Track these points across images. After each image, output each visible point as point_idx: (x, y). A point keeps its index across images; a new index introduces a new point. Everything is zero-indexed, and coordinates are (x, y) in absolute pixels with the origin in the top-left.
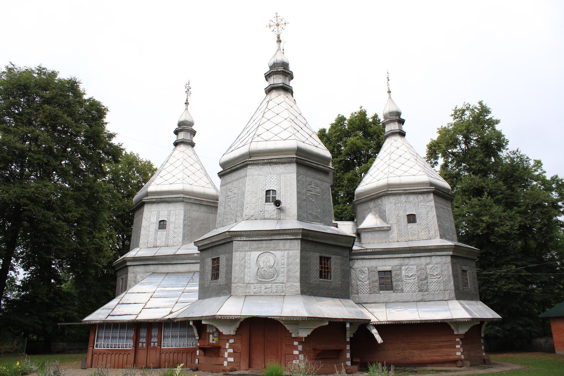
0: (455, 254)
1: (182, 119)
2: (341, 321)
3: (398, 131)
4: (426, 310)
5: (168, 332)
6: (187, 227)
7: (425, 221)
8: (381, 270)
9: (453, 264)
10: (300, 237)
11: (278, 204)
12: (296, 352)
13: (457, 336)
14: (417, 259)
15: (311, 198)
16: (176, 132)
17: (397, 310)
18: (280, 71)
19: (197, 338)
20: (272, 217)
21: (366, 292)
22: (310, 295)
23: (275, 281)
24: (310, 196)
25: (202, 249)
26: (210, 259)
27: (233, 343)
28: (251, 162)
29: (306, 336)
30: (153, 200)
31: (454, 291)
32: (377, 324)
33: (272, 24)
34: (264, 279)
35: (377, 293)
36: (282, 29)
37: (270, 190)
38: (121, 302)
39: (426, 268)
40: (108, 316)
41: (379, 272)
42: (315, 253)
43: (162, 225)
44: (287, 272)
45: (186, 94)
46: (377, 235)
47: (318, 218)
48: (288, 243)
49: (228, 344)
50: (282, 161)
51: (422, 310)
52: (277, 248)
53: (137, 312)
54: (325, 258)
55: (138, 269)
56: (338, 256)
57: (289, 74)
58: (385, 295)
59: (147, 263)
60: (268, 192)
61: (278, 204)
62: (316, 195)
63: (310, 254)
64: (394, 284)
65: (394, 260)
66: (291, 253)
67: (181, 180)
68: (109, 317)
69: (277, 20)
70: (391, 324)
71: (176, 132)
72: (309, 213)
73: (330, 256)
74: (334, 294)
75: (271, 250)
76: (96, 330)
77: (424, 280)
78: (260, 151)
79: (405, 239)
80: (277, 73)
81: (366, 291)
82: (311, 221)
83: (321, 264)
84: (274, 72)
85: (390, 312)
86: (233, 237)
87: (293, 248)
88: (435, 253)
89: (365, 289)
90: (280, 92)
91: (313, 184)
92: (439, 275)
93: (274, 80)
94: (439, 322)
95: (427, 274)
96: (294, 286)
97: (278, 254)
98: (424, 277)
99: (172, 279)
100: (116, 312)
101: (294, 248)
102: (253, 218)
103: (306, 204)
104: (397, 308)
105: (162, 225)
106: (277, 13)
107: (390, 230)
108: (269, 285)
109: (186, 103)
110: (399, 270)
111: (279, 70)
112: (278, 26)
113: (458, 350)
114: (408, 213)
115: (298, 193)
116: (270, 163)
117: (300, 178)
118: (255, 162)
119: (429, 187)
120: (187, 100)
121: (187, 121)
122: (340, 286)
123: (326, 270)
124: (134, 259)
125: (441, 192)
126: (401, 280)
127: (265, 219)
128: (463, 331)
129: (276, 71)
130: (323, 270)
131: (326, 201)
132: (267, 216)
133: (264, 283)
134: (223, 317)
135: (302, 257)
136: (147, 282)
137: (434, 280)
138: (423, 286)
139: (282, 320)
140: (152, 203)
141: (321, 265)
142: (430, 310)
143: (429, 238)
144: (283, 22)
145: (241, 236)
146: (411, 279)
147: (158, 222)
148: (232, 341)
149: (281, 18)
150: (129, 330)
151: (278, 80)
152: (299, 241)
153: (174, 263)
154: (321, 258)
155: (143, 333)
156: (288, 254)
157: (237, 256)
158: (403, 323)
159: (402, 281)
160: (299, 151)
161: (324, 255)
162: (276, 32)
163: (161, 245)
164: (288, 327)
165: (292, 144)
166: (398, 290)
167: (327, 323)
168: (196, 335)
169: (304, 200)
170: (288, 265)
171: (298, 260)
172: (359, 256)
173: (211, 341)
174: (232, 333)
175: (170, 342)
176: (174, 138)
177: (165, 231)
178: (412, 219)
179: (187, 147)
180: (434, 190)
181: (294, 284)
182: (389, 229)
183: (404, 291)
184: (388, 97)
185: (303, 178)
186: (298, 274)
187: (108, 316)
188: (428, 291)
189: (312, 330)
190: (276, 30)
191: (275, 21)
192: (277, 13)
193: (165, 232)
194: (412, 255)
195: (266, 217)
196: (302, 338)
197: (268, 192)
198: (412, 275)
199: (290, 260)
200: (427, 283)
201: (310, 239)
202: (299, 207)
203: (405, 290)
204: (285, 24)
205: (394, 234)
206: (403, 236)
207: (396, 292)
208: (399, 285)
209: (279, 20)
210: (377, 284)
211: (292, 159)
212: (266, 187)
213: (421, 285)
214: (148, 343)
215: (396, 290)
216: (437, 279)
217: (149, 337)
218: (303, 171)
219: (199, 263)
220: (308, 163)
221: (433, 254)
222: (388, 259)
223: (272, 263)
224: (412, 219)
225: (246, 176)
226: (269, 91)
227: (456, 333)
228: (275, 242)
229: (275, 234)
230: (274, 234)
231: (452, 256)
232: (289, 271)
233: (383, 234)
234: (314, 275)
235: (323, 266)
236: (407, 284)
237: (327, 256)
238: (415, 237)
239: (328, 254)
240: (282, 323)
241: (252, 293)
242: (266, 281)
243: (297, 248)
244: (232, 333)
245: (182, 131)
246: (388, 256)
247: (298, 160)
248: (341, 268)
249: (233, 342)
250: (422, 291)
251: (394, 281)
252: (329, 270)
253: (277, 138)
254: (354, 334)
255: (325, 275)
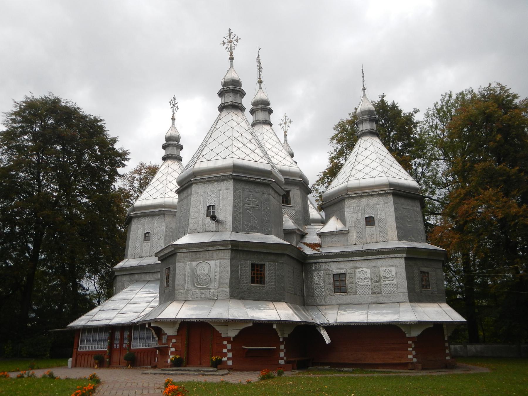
0: (409, 256)
1: (168, 135)
2: (266, 322)
3: (369, 130)
4: (376, 312)
5: (136, 334)
6: (169, 237)
7: (383, 223)
8: (335, 273)
9: (407, 266)
10: (230, 248)
11: (214, 219)
12: (225, 351)
13: (411, 339)
14: (337, 263)
15: (248, 211)
16: (164, 147)
17: (348, 312)
18: (229, 90)
19: (157, 339)
20: (212, 230)
21: (365, 293)
22: (240, 299)
23: (209, 288)
24: (247, 208)
25: (162, 259)
26: (165, 268)
27: (175, 342)
28: (194, 182)
29: (234, 336)
30: (139, 215)
31: (407, 294)
32: (326, 325)
33: (225, 41)
34: (201, 285)
35: (332, 296)
36: (234, 46)
37: (210, 206)
38: (102, 309)
39: (380, 271)
40: (89, 321)
41: (334, 275)
42: (246, 261)
43: (147, 236)
44: (219, 279)
45: (171, 110)
46: (336, 239)
47: (255, 228)
48: (220, 254)
49: (171, 344)
50: (221, 178)
51: (373, 312)
52: (211, 258)
53: (113, 316)
54: (257, 265)
55: (125, 278)
56: (272, 263)
57: (240, 91)
58: (340, 297)
59: (131, 272)
60: (209, 207)
61: (214, 219)
62: (253, 207)
63: (241, 262)
64: (348, 286)
65: (348, 263)
66: (223, 262)
67: (164, 194)
68: (89, 322)
69: (230, 37)
70: (337, 326)
71: (164, 147)
72: (245, 225)
73: (264, 263)
74: (267, 297)
75: (207, 260)
76: (132, 331)
77: (378, 282)
78: (202, 170)
79: (363, 242)
80: (227, 91)
81: (392, 288)
82: (247, 232)
83: (252, 270)
84: (224, 91)
85: (341, 314)
86: (177, 249)
87: (224, 258)
88: (388, 255)
89: (394, 289)
90: (229, 110)
91: (251, 197)
92: (392, 277)
93: (225, 99)
94: (386, 324)
95: (380, 276)
96: (224, 291)
97: (212, 263)
98: (377, 280)
99: (151, 286)
100: (96, 317)
101: (225, 258)
102: (196, 231)
103: (243, 217)
104: (349, 311)
105: (147, 236)
106: (230, 30)
107: (349, 233)
108: (203, 291)
109: (258, 82)
110: (353, 272)
111: (228, 89)
112: (231, 43)
113: (410, 353)
114: (366, 216)
115: (234, 207)
116: (210, 181)
117: (237, 193)
118: (198, 181)
119: (389, 189)
120: (260, 78)
121: (172, 136)
122: (274, 290)
123: (259, 276)
124: (122, 269)
125: (402, 193)
126: (354, 283)
127: (206, 232)
128: (415, 333)
129: (226, 90)
130: (256, 276)
131: (265, 211)
132: (208, 229)
133: (201, 289)
134: (161, 320)
135: (231, 266)
136: (129, 289)
137: (387, 283)
138: (376, 288)
139: (210, 322)
140: (139, 217)
141: (253, 272)
142: (380, 312)
143: (387, 240)
144: (235, 38)
145: (182, 248)
146: (364, 282)
147: (143, 235)
148: (174, 341)
149: (233, 34)
150: (135, 332)
151: (229, 99)
152: (230, 251)
153: (154, 271)
154: (253, 265)
155: (126, 334)
156: (220, 263)
157: (179, 265)
158: (351, 325)
159: (356, 283)
160: (236, 168)
161: (256, 262)
162: (229, 49)
163: (146, 256)
164: (217, 328)
165: (228, 162)
166: (351, 293)
167: (432, 326)
168: (155, 336)
169: (240, 213)
170: (220, 272)
171: (228, 269)
172: (315, 260)
173: (164, 342)
174: (175, 334)
175: (145, 343)
176: (163, 153)
177: (149, 242)
178: (370, 221)
179: (172, 161)
180: (392, 191)
181: (225, 289)
182: (347, 232)
183: (357, 293)
184: (362, 95)
185: (241, 193)
186: (228, 281)
187: (89, 321)
188: (381, 294)
189: (239, 331)
190: (229, 47)
191: (228, 38)
192: (230, 30)
193: (149, 244)
194: (365, 258)
195: (207, 230)
196: (230, 338)
197: (209, 207)
198: (365, 278)
199: (221, 268)
200: (381, 285)
201: (240, 248)
202: (235, 219)
203: (359, 292)
204: (237, 40)
205: (353, 237)
206: (361, 239)
207: (349, 294)
208: (353, 288)
209: (232, 36)
210: (332, 287)
211: (229, 177)
212: (208, 203)
213: (375, 287)
214: (121, 344)
215: (349, 292)
216: (390, 281)
217: (122, 339)
218: (240, 186)
219: (160, 272)
220: (244, 178)
221: (386, 256)
222: (373, 260)
223: (206, 272)
224: (370, 221)
225: (191, 194)
226: (222, 108)
227: (407, 335)
228: (210, 252)
229: (209, 246)
230: (218, 245)
231: (405, 258)
232: (220, 278)
233: (342, 238)
234: (244, 281)
235: (256, 272)
236: (361, 286)
237: (260, 263)
238: (374, 240)
239: (261, 261)
240: (211, 324)
241: (190, 299)
242: (202, 287)
243: (227, 257)
244: (175, 334)
245: (168, 147)
246: (342, 259)
247: (234, 177)
248: (275, 273)
249: (175, 341)
250: (375, 294)
251: (348, 283)
252: (262, 276)
253: (218, 157)
254: (289, 335)
255: (257, 281)
